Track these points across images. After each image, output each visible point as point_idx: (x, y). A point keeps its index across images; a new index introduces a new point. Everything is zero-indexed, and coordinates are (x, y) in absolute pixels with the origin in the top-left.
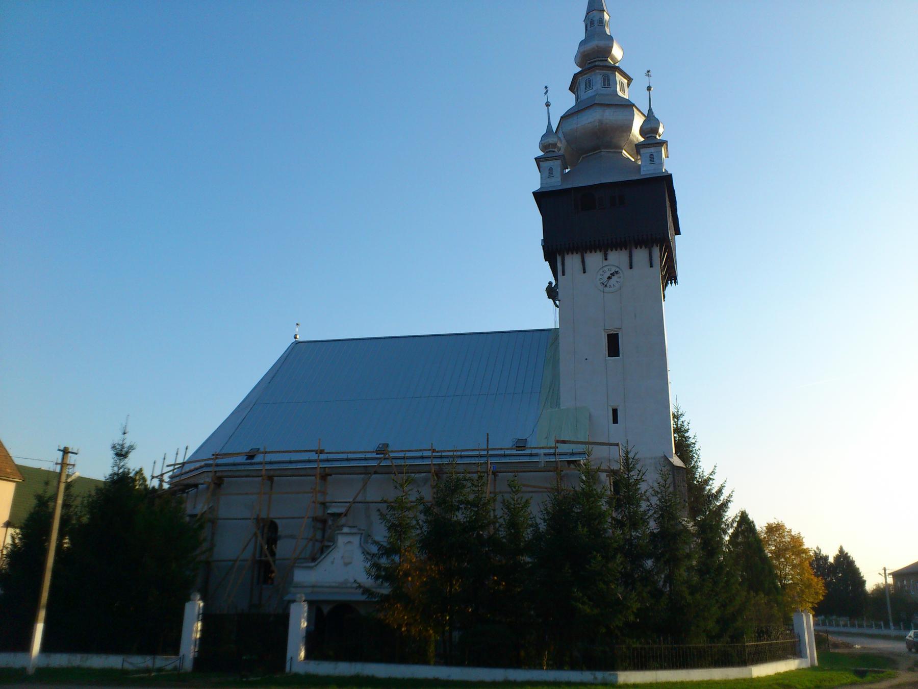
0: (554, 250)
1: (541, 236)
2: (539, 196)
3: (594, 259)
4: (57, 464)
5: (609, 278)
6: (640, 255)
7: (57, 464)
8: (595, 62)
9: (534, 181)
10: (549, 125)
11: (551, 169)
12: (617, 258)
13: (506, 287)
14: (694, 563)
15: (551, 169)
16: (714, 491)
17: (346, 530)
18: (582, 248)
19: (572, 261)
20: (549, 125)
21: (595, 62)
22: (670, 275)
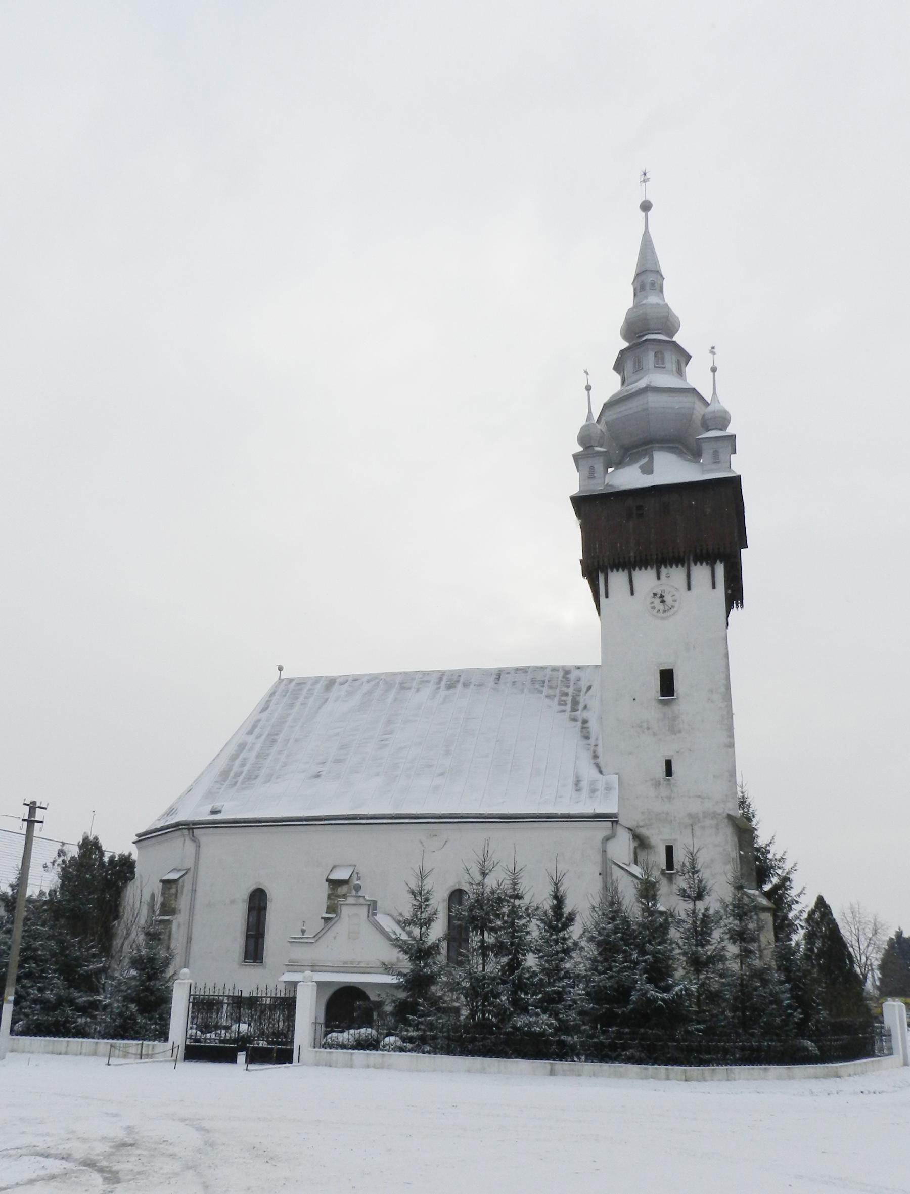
0: (595, 568)
1: (580, 556)
2: (581, 503)
3: (645, 579)
4: (24, 820)
5: (663, 602)
6: (701, 573)
7: (24, 820)
8: (648, 278)
9: (572, 483)
10: (590, 412)
11: (592, 468)
12: (675, 576)
13: (540, 599)
14: (40, 953)
15: (592, 468)
16: (720, 889)
17: (350, 900)
18: (628, 564)
19: (617, 580)
20: (590, 412)
21: (648, 278)
22: (735, 595)
